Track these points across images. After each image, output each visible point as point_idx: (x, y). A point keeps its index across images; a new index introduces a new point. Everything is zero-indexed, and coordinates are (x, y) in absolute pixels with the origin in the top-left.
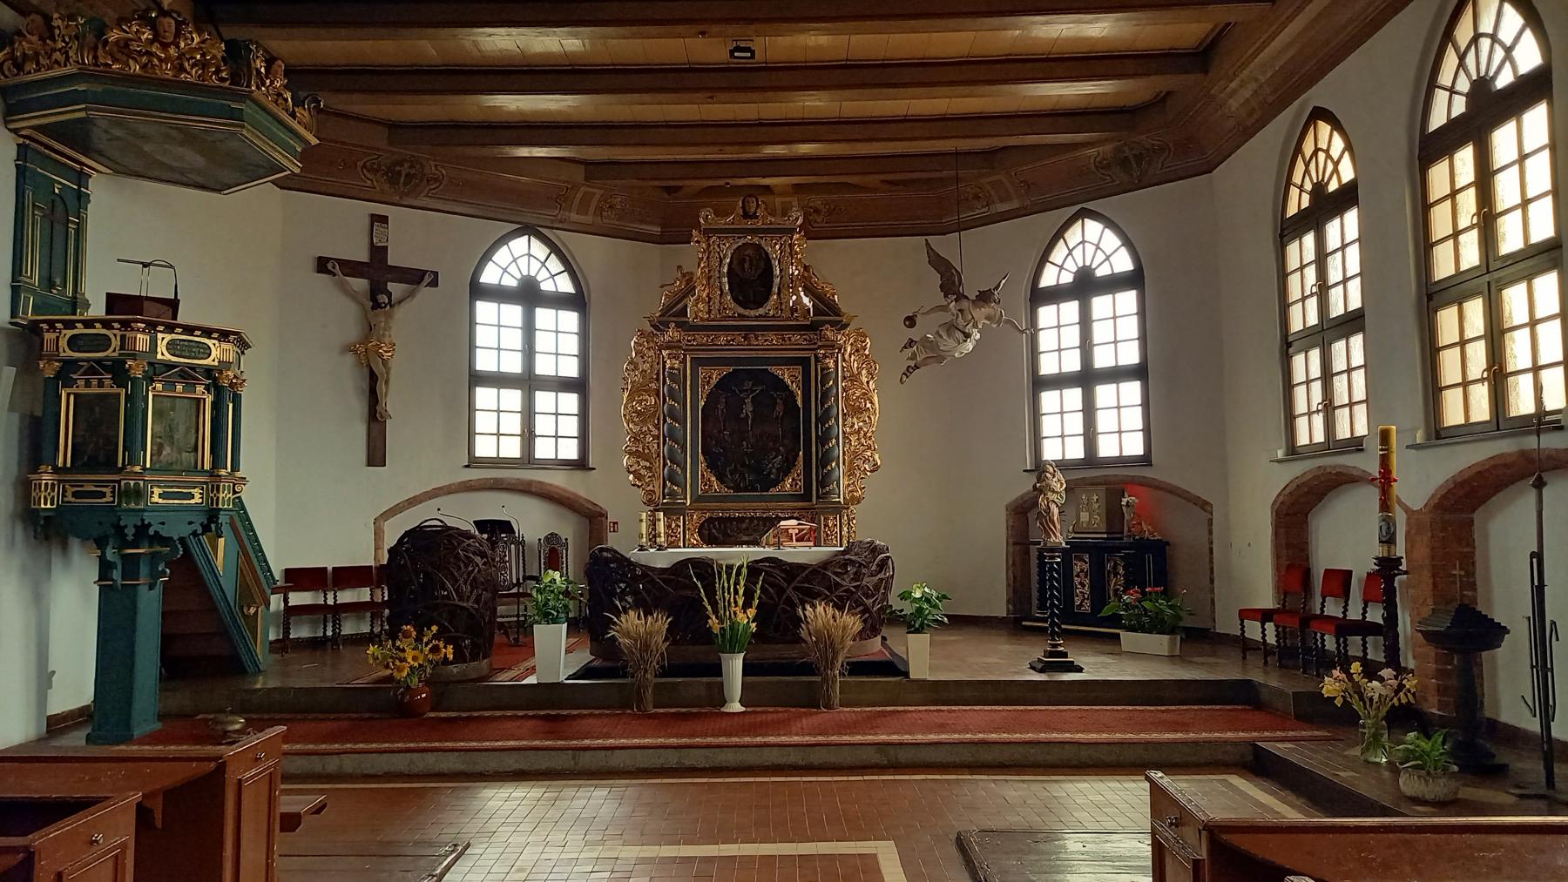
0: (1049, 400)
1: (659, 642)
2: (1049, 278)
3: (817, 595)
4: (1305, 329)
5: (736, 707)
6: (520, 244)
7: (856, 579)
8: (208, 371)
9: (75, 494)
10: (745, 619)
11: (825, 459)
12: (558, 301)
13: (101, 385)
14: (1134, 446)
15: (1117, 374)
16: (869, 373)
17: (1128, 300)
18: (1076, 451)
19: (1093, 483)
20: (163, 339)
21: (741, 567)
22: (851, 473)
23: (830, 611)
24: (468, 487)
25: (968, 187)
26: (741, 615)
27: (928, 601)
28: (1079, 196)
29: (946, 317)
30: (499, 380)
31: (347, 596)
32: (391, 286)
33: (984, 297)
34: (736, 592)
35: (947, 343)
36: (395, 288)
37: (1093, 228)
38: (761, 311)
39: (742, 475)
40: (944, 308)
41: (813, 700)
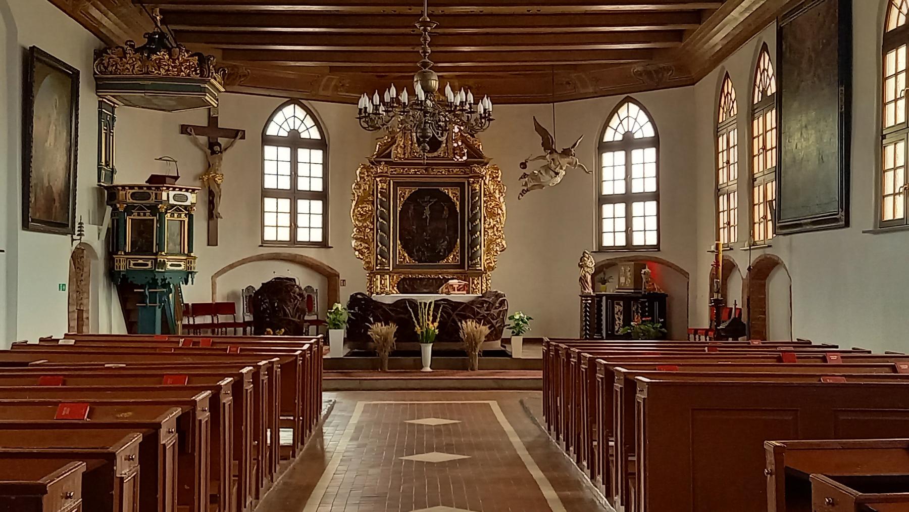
0: (607, 209)
1: (392, 339)
2: (609, 137)
3: (469, 318)
4: (896, 125)
5: (429, 369)
6: (289, 110)
7: (489, 309)
8: (186, 207)
9: (134, 265)
10: (433, 327)
11: (473, 244)
12: (311, 144)
13: (145, 215)
14: (652, 240)
15: (644, 197)
16: (500, 192)
17: (651, 153)
18: (621, 241)
19: (629, 260)
20: (172, 194)
21: (431, 303)
22: (488, 251)
23: (474, 324)
24: (260, 258)
25: (558, 79)
26: (431, 325)
27: (522, 320)
28: (627, 90)
29: (544, 163)
30: (277, 194)
31: (199, 320)
32: (220, 140)
33: (566, 153)
34: (429, 314)
35: (545, 178)
36: (222, 141)
37: (634, 108)
38: (436, 154)
39: (423, 252)
40: (544, 157)
41: (465, 367)
